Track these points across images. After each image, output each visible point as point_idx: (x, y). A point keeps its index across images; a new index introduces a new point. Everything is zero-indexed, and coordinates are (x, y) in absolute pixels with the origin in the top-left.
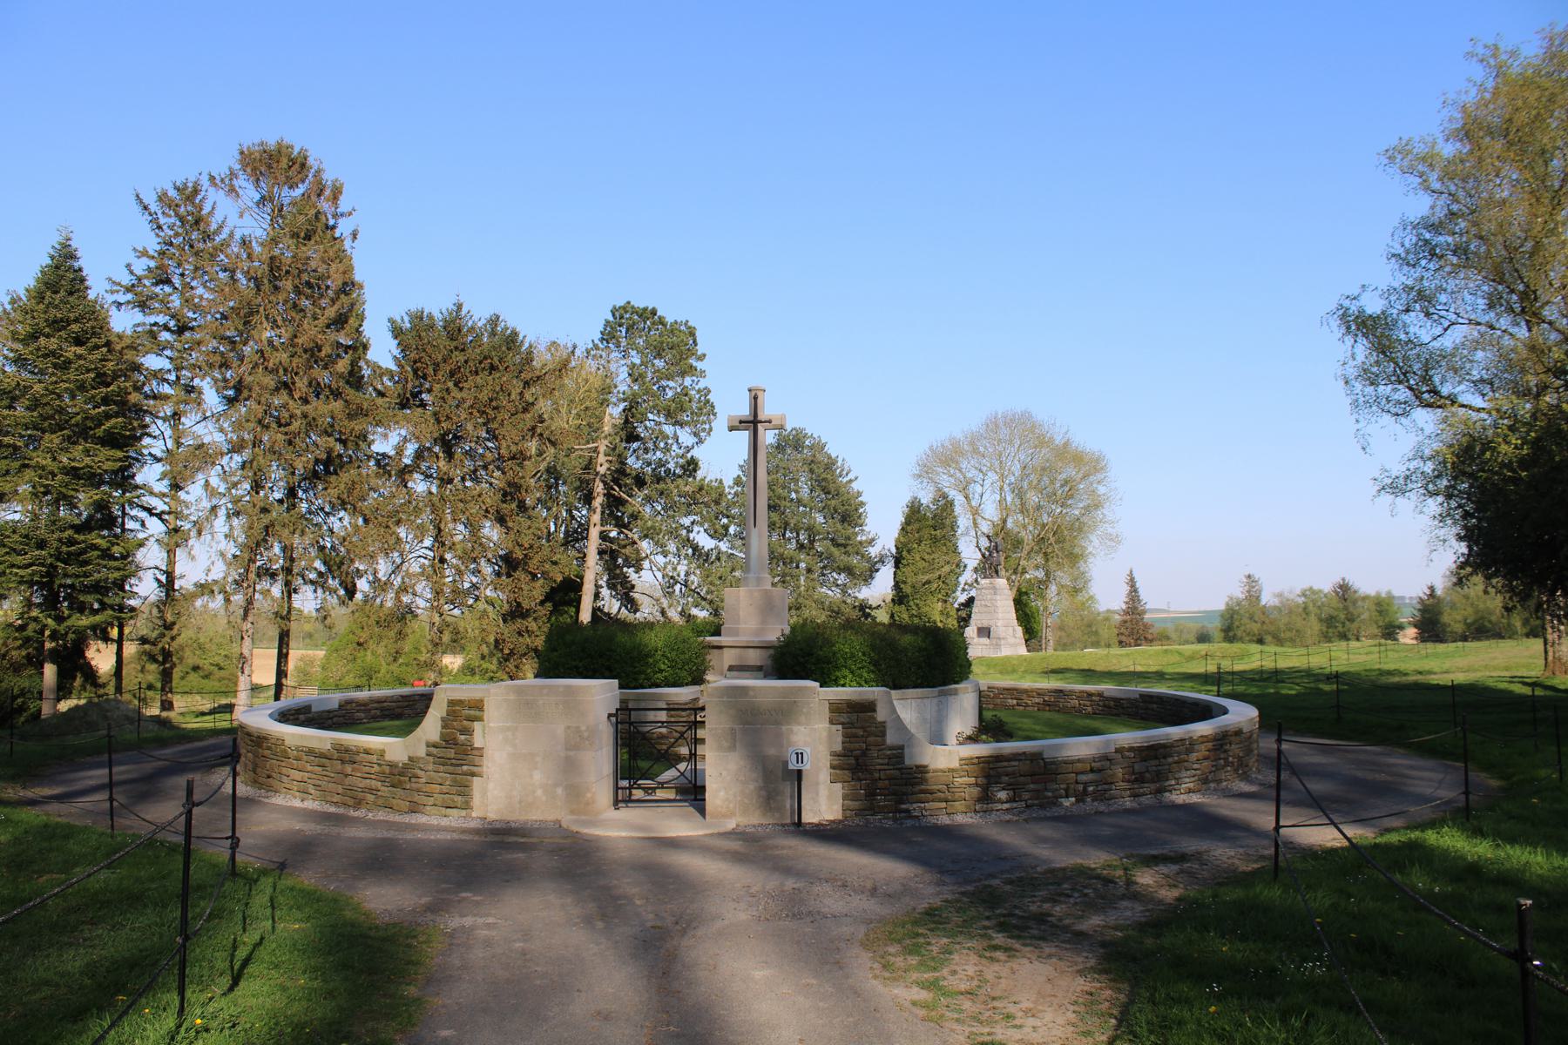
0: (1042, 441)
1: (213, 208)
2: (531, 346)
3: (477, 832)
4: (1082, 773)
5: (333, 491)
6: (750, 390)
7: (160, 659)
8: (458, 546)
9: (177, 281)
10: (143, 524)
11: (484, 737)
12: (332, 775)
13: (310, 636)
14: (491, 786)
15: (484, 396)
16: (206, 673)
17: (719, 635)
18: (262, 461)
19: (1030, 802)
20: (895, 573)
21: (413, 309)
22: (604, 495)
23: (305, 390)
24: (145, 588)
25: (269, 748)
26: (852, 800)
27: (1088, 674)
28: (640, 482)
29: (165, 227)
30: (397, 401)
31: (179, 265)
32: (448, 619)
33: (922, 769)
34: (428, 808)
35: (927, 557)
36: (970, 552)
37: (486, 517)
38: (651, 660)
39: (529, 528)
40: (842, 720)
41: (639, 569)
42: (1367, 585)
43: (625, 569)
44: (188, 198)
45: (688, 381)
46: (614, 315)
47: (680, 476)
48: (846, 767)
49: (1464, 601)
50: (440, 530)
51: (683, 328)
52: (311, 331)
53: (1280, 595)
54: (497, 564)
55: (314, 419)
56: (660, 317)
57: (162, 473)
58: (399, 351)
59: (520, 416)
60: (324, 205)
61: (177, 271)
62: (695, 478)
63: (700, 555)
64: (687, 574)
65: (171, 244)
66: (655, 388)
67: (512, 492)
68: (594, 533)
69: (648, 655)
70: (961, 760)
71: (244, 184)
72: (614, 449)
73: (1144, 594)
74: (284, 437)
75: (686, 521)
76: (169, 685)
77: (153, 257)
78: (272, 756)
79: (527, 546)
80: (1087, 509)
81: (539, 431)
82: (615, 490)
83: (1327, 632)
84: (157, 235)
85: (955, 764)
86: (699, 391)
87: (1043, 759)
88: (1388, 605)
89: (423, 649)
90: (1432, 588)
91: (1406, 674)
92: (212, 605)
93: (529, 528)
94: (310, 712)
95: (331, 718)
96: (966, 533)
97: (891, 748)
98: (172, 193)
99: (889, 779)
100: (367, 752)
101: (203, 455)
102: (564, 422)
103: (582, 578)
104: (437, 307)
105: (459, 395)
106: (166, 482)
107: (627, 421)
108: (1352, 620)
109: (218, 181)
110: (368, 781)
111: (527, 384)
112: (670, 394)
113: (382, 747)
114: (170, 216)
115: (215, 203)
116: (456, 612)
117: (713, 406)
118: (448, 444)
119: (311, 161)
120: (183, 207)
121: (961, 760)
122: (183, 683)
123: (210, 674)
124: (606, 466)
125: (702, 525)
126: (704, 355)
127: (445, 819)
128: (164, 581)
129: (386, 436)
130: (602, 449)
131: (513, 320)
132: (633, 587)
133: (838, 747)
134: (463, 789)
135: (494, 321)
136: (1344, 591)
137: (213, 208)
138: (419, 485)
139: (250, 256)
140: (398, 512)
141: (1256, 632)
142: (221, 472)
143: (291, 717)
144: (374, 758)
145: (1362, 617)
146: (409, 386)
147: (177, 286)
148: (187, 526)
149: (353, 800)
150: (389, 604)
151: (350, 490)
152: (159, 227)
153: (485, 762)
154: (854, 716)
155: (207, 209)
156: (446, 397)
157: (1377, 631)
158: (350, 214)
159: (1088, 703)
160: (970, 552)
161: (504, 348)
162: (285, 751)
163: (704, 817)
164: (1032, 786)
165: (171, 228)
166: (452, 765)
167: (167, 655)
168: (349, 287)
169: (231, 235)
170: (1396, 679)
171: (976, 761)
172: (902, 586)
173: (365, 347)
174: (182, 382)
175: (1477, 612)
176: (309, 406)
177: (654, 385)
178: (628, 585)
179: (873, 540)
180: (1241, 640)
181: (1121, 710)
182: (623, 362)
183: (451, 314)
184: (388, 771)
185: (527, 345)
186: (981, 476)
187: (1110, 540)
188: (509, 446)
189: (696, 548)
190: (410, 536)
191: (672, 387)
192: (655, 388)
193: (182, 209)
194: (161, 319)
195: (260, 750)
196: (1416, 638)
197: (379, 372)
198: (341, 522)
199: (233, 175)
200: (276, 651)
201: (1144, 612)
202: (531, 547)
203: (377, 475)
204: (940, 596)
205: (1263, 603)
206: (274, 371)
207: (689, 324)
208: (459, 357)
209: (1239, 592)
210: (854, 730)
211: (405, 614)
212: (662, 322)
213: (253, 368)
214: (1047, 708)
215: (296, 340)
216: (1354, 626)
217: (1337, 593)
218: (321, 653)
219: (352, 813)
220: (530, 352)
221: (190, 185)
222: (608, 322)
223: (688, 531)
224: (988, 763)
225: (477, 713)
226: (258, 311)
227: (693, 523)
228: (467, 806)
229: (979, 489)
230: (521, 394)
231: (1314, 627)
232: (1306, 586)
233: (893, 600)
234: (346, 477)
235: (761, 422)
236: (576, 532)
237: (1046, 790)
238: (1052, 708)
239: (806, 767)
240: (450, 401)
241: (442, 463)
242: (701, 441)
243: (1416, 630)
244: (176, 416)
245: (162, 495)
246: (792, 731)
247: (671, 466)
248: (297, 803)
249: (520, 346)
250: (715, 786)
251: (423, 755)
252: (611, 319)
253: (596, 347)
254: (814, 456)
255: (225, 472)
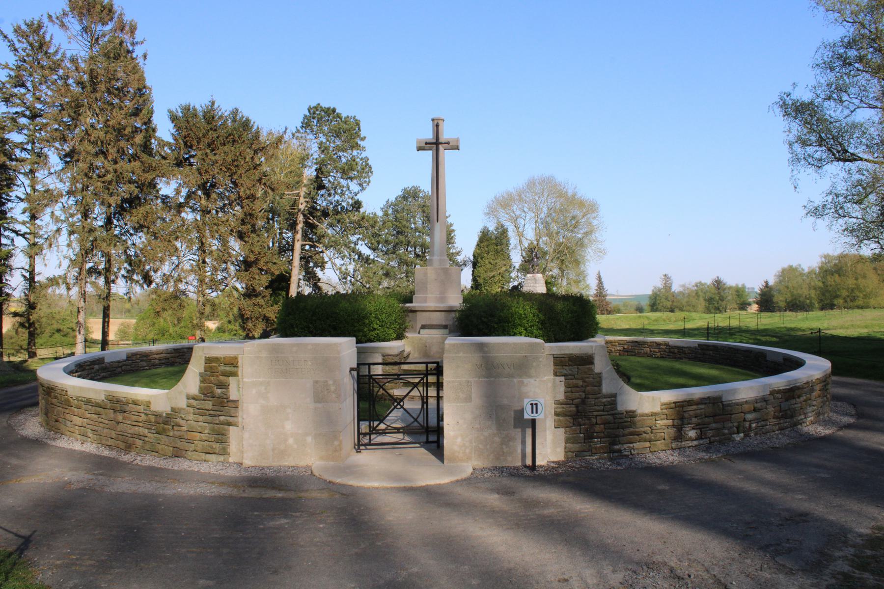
0: (561, 194)
1: (51, 39)
2: (258, 128)
3: (234, 482)
4: (749, 412)
5: (134, 218)
6: (433, 120)
7: (27, 325)
8: (214, 253)
9: (29, 85)
10: (13, 240)
11: (239, 390)
12: (107, 422)
13: (129, 311)
14: (246, 435)
15: (229, 159)
16: (65, 333)
17: (411, 302)
18: (88, 200)
19: (712, 439)
20: (473, 271)
21: (184, 104)
22: (304, 222)
23: (115, 155)
24: (16, 282)
25: (56, 397)
26: (573, 443)
27: (684, 333)
28: (325, 214)
29: (20, 50)
30: (175, 162)
31: (31, 75)
32: (209, 297)
33: (631, 414)
34: (189, 453)
35: (492, 262)
36: (516, 258)
37: (231, 234)
38: (367, 321)
39: (258, 241)
40: (565, 372)
41: (323, 268)
42: (731, 280)
43: (315, 269)
44: (34, 31)
45: (355, 153)
46: (309, 112)
47: (350, 211)
48: (569, 414)
49: (786, 290)
50: (202, 244)
51: (352, 120)
52: (118, 117)
53: (684, 286)
54: (238, 265)
55: (121, 173)
56: (337, 114)
57: (24, 209)
58: (175, 130)
59: (252, 171)
60: (126, 37)
61: (29, 79)
62: (359, 211)
63: (363, 259)
64: (355, 271)
65: (25, 61)
66: (335, 157)
67: (248, 218)
68: (298, 246)
69: (365, 317)
70: (662, 405)
71: (72, 20)
72: (310, 194)
73: (606, 285)
74: (102, 184)
75: (354, 238)
76: (33, 342)
77: (13, 69)
78: (58, 404)
79: (257, 253)
80: (586, 234)
81: (263, 181)
82: (310, 219)
83: (709, 307)
84: (15, 55)
85: (657, 409)
86: (362, 159)
87: (722, 402)
88: (742, 291)
89: (195, 318)
90: (767, 283)
91: (804, 330)
92: (57, 292)
93: (258, 241)
94: (103, 363)
95: (121, 367)
96: (515, 248)
97: (606, 396)
98: (24, 27)
99: (604, 424)
100: (135, 403)
101: (50, 197)
102: (280, 176)
103: (290, 274)
104: (199, 103)
105: (214, 158)
106: (27, 214)
107: (317, 177)
108: (722, 300)
109: (54, 19)
110: (137, 428)
111: (256, 152)
112: (344, 160)
113: (147, 399)
114: (23, 43)
115: (52, 35)
116: (214, 294)
117: (370, 167)
118: (207, 189)
119: (115, 7)
120: (31, 36)
121: (662, 405)
122: (52, 339)
123: (67, 334)
124: (305, 204)
125: (364, 241)
126: (365, 138)
127: (205, 464)
128: (28, 277)
129: (168, 183)
130: (302, 194)
131: (246, 112)
132: (319, 279)
133: (561, 397)
134: (220, 437)
135: (235, 112)
136: (718, 284)
137: (51, 39)
138: (188, 216)
139: (77, 69)
140: (176, 232)
141: (669, 307)
142: (62, 207)
143: (88, 367)
144: (141, 408)
145: (728, 298)
146: (182, 152)
147: (30, 88)
148: (40, 241)
149: (124, 444)
150: (171, 289)
151: (146, 217)
152: (16, 50)
153: (240, 413)
154: (575, 369)
155: (48, 39)
156: (205, 158)
157: (736, 306)
158: (142, 43)
159: (657, 350)
160: (516, 258)
161: (241, 129)
162: (69, 401)
163: (443, 462)
164: (714, 425)
165: (24, 50)
166: (210, 415)
167: (32, 325)
168: (142, 91)
169: (64, 55)
170: (801, 333)
171: (673, 405)
172: (478, 279)
173: (154, 130)
174: (36, 151)
175: (792, 296)
176: (118, 165)
177: (334, 155)
178: (316, 278)
179: (459, 252)
180: (660, 311)
181: (683, 355)
182: (315, 141)
183: (207, 107)
184: (153, 420)
185: (255, 127)
186: (524, 214)
187: (599, 252)
188: (245, 191)
189: (360, 255)
190: (184, 246)
191: (345, 157)
192: (335, 157)
193: (31, 39)
194: (19, 109)
195: (50, 399)
196: (758, 310)
197: (162, 144)
198: (140, 239)
199: (65, 14)
200: (102, 320)
201: (606, 295)
202: (259, 254)
203: (163, 209)
204: (500, 285)
205: (673, 290)
206: (94, 143)
207: (356, 118)
208: (213, 135)
209: (659, 284)
210: (575, 381)
211: (177, 296)
212: (339, 116)
213: (81, 141)
214: (626, 354)
215: (108, 123)
216: (724, 303)
217: (714, 285)
218: (134, 321)
219: (126, 458)
220: (258, 132)
221: (36, 22)
222: (305, 116)
223: (355, 244)
224: (683, 406)
225: (232, 369)
226: (83, 105)
227: (358, 239)
228: (224, 452)
229: (523, 222)
230: (252, 158)
231: (702, 304)
232: (698, 280)
233: (472, 287)
234: (142, 210)
235: (442, 143)
236: (285, 247)
237: (724, 428)
238: (629, 353)
239: (539, 417)
240: (208, 161)
241: (203, 202)
242: (363, 189)
243: (757, 306)
244: (32, 171)
245: (24, 223)
246: (522, 382)
247: (344, 204)
248: (77, 446)
249: (251, 128)
250: (452, 433)
251: (185, 406)
252: (308, 114)
253: (298, 131)
254: (425, 202)
255: (64, 207)
